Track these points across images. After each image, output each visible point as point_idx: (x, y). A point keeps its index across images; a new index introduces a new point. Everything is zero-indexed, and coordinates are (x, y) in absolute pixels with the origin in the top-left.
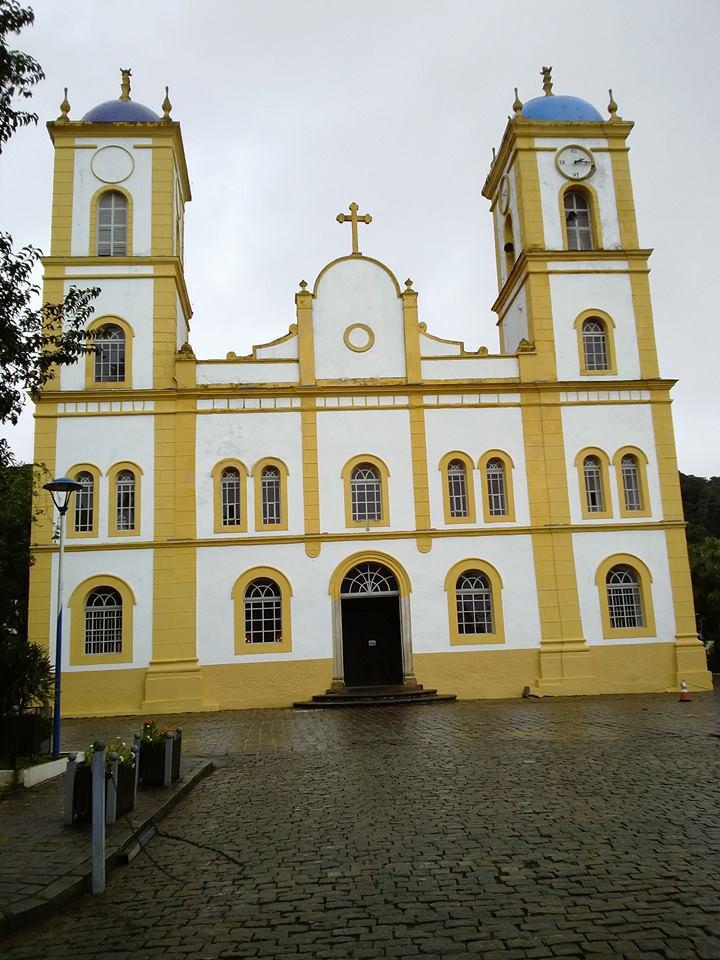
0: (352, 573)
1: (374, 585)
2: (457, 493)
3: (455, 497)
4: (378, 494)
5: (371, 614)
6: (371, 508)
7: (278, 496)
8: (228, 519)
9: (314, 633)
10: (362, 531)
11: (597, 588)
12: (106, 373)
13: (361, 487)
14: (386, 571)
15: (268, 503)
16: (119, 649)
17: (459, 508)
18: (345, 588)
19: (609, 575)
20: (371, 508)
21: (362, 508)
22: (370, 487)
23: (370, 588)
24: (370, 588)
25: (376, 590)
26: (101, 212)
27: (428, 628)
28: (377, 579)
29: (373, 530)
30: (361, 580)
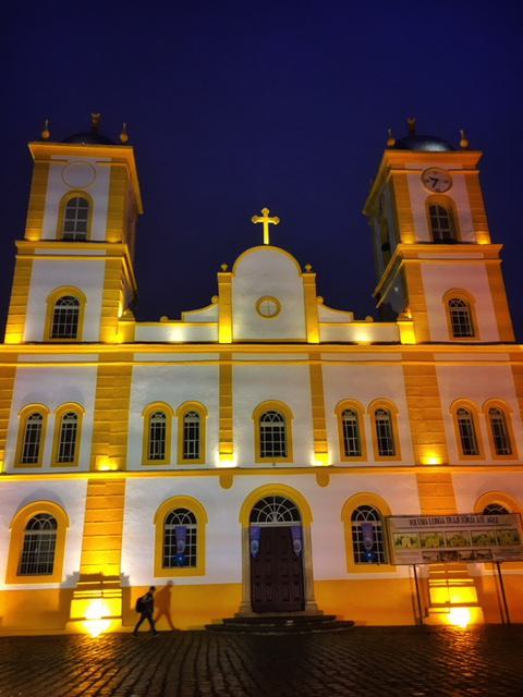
0: (260, 504)
1: (278, 516)
2: (350, 435)
3: (348, 439)
4: (283, 435)
5: (276, 542)
6: (277, 447)
7: (74, 437)
8: (349, 451)
9: (225, 558)
10: (270, 465)
11: (154, 526)
12: (61, 331)
13: (268, 429)
14: (289, 504)
15: (189, 441)
16: (194, 563)
17: (352, 449)
18: (253, 517)
19: (355, 513)
20: (277, 447)
21: (269, 447)
22: (276, 429)
23: (275, 518)
24: (275, 518)
25: (281, 520)
26: (85, 217)
27: (327, 555)
28: (282, 510)
29: (278, 465)
30: (268, 510)
